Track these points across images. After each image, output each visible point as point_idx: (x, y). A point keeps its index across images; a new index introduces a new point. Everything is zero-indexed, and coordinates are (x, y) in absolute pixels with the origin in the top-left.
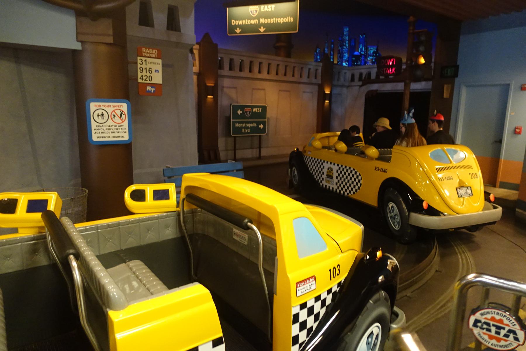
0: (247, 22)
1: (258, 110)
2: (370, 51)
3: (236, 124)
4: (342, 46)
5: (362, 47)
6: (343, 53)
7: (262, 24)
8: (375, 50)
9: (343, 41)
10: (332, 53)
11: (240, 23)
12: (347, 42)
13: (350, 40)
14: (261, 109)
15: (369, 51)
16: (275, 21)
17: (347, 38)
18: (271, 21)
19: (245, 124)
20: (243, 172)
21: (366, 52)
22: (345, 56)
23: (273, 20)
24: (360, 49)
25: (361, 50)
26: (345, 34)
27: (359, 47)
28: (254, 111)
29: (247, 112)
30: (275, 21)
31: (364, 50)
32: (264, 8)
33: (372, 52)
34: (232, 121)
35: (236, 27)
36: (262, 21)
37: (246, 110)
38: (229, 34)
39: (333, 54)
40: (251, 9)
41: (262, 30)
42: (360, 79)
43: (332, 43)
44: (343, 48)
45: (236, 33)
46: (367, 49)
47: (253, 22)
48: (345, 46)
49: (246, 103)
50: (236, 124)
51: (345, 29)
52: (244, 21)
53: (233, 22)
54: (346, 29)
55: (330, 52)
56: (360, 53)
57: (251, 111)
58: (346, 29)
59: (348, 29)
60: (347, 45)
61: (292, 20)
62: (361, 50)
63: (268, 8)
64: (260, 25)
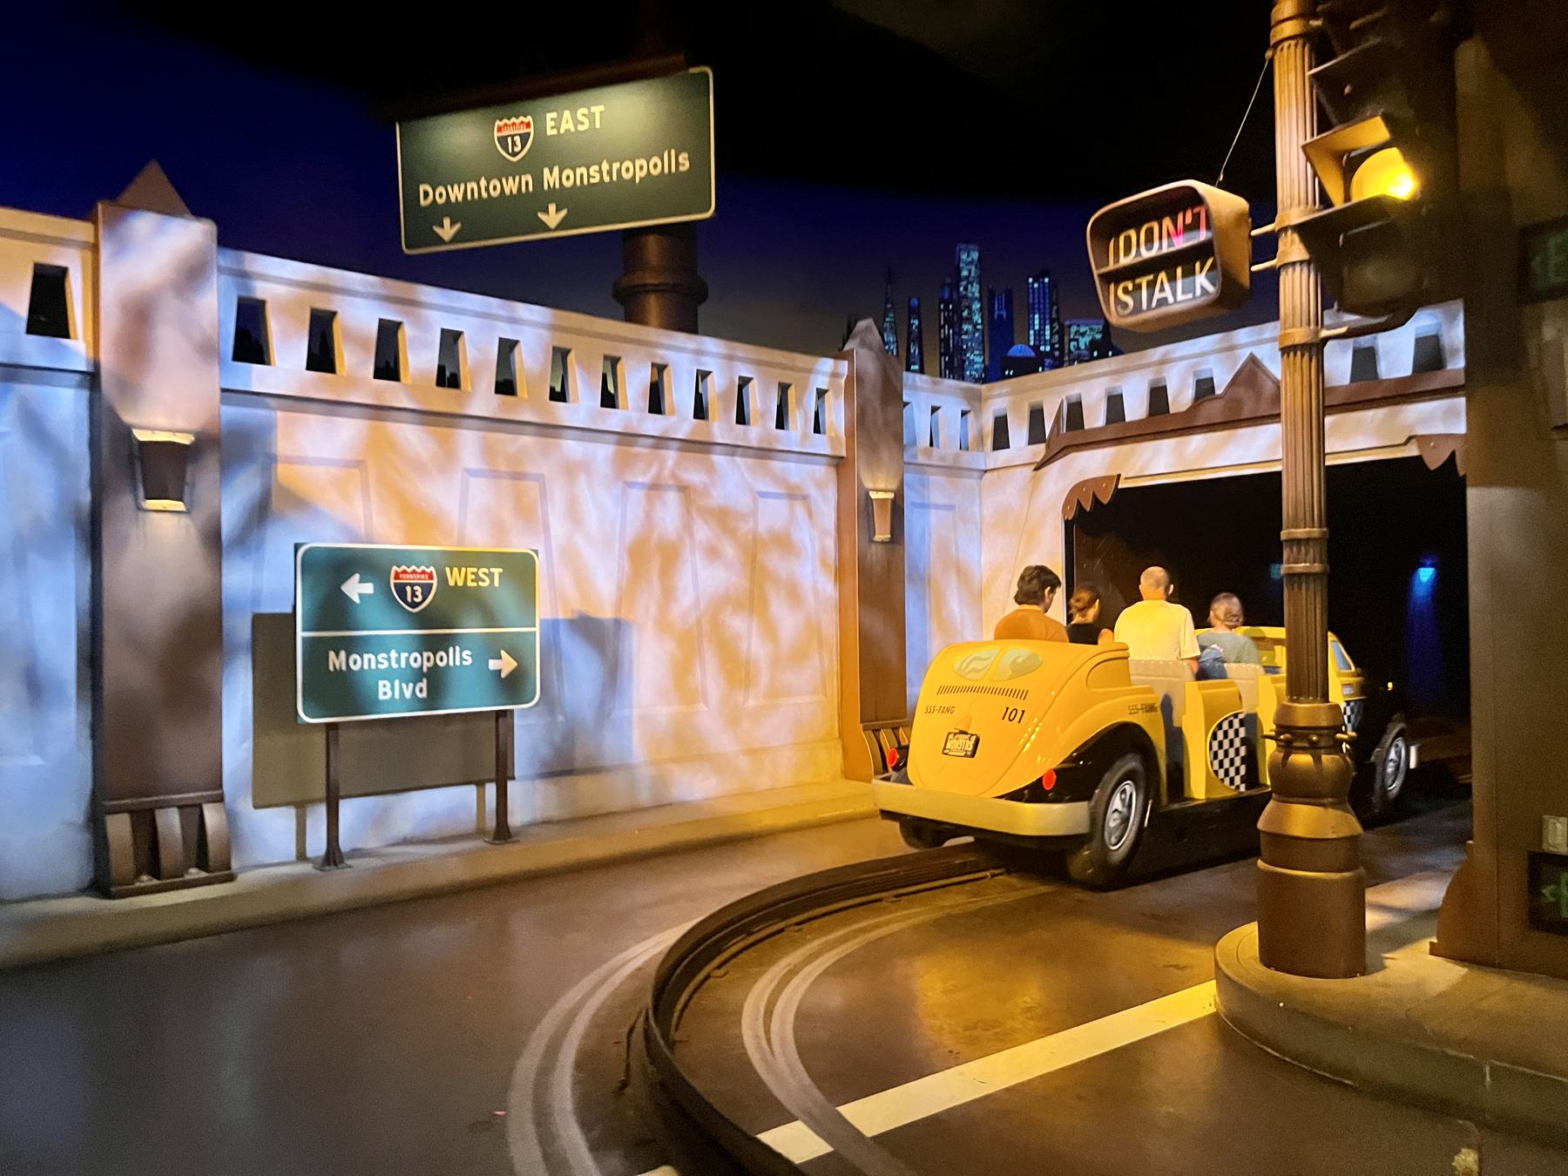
0: (487, 189)
1: (478, 579)
2: (1077, 340)
3: (332, 654)
4: (956, 321)
5: (1042, 325)
6: (966, 351)
7: (552, 190)
8: (1099, 336)
9: (960, 302)
10: (914, 349)
11: (456, 194)
12: (976, 306)
13: (988, 297)
14: (497, 571)
15: (1071, 340)
16: (610, 173)
17: (975, 290)
18: (589, 176)
19: (393, 654)
20: (1461, 402)
21: (1061, 341)
22: (972, 363)
23: (600, 172)
24: (1032, 332)
25: (1039, 334)
26: (965, 273)
27: (1030, 325)
28: (452, 583)
29: (408, 589)
30: (610, 173)
31: (1052, 335)
32: (558, 122)
33: (1084, 342)
34: (304, 639)
35: (437, 213)
36: (551, 178)
37: (397, 576)
38: (407, 247)
39: (921, 353)
40: (500, 129)
41: (553, 217)
42: (1036, 435)
43: (915, 312)
44: (959, 333)
45: (440, 241)
46: (1061, 332)
47: (511, 186)
48: (969, 320)
49: (506, 547)
50: (332, 654)
51: (964, 256)
52: (472, 185)
53: (426, 194)
54: (969, 258)
55: (909, 350)
56: (1036, 348)
57: (435, 582)
58: (969, 258)
59: (975, 255)
60: (977, 318)
61: (685, 165)
62: (1039, 334)
63: (576, 122)
64: (541, 198)
